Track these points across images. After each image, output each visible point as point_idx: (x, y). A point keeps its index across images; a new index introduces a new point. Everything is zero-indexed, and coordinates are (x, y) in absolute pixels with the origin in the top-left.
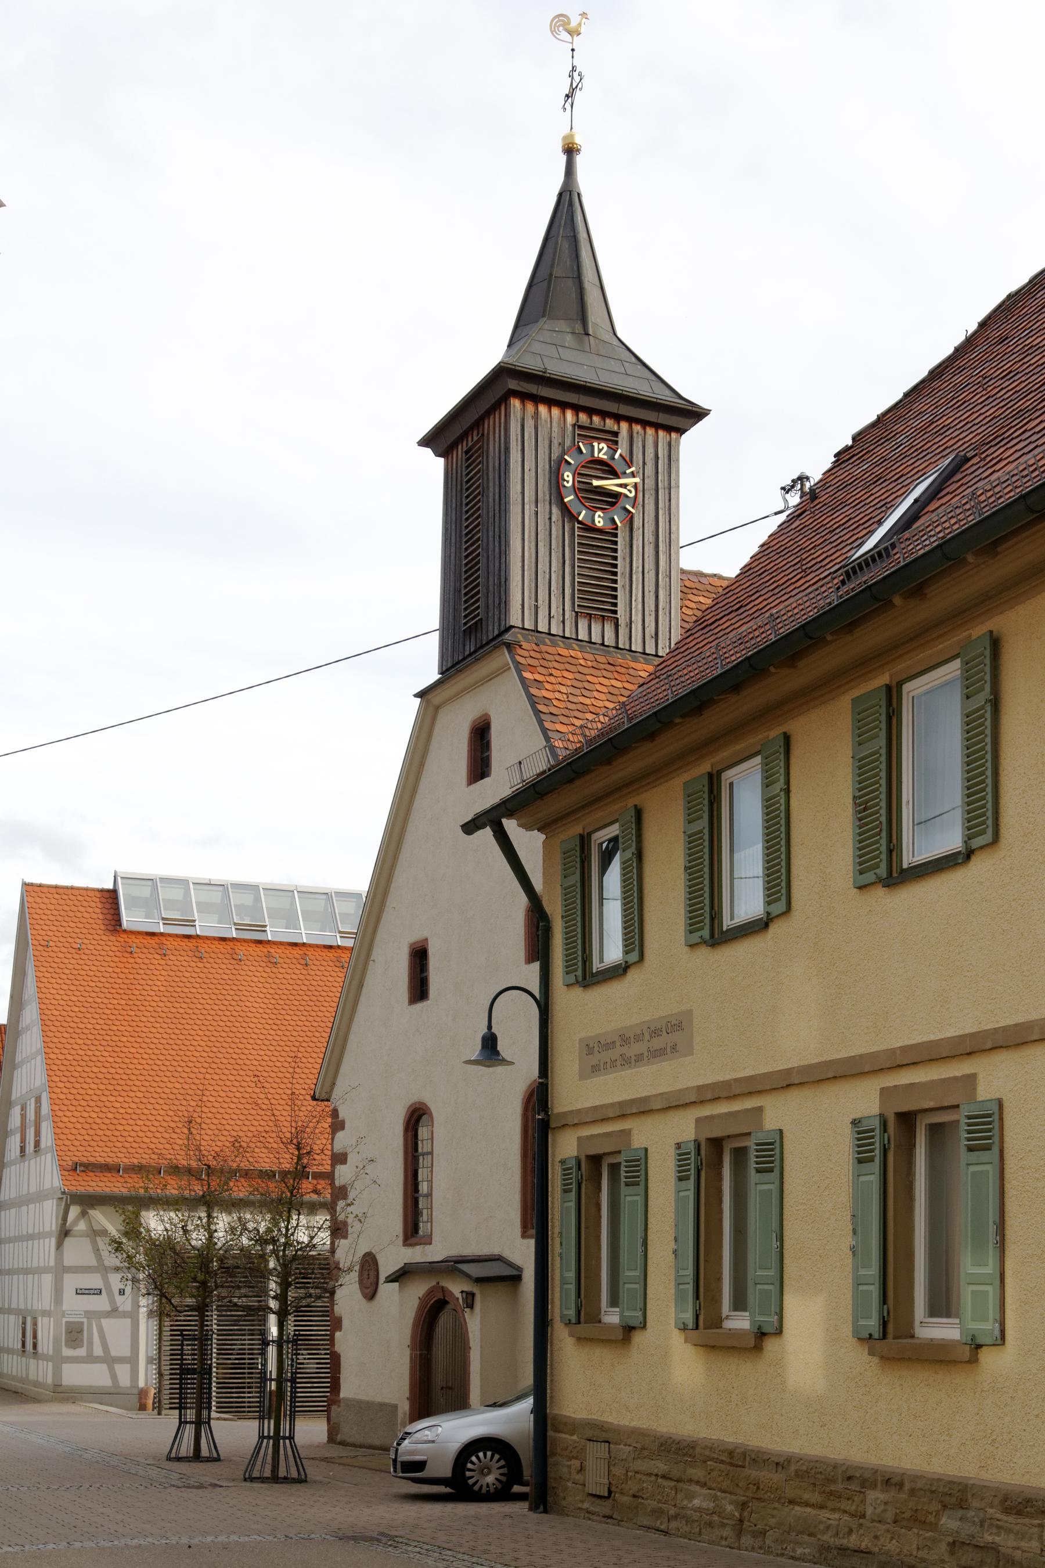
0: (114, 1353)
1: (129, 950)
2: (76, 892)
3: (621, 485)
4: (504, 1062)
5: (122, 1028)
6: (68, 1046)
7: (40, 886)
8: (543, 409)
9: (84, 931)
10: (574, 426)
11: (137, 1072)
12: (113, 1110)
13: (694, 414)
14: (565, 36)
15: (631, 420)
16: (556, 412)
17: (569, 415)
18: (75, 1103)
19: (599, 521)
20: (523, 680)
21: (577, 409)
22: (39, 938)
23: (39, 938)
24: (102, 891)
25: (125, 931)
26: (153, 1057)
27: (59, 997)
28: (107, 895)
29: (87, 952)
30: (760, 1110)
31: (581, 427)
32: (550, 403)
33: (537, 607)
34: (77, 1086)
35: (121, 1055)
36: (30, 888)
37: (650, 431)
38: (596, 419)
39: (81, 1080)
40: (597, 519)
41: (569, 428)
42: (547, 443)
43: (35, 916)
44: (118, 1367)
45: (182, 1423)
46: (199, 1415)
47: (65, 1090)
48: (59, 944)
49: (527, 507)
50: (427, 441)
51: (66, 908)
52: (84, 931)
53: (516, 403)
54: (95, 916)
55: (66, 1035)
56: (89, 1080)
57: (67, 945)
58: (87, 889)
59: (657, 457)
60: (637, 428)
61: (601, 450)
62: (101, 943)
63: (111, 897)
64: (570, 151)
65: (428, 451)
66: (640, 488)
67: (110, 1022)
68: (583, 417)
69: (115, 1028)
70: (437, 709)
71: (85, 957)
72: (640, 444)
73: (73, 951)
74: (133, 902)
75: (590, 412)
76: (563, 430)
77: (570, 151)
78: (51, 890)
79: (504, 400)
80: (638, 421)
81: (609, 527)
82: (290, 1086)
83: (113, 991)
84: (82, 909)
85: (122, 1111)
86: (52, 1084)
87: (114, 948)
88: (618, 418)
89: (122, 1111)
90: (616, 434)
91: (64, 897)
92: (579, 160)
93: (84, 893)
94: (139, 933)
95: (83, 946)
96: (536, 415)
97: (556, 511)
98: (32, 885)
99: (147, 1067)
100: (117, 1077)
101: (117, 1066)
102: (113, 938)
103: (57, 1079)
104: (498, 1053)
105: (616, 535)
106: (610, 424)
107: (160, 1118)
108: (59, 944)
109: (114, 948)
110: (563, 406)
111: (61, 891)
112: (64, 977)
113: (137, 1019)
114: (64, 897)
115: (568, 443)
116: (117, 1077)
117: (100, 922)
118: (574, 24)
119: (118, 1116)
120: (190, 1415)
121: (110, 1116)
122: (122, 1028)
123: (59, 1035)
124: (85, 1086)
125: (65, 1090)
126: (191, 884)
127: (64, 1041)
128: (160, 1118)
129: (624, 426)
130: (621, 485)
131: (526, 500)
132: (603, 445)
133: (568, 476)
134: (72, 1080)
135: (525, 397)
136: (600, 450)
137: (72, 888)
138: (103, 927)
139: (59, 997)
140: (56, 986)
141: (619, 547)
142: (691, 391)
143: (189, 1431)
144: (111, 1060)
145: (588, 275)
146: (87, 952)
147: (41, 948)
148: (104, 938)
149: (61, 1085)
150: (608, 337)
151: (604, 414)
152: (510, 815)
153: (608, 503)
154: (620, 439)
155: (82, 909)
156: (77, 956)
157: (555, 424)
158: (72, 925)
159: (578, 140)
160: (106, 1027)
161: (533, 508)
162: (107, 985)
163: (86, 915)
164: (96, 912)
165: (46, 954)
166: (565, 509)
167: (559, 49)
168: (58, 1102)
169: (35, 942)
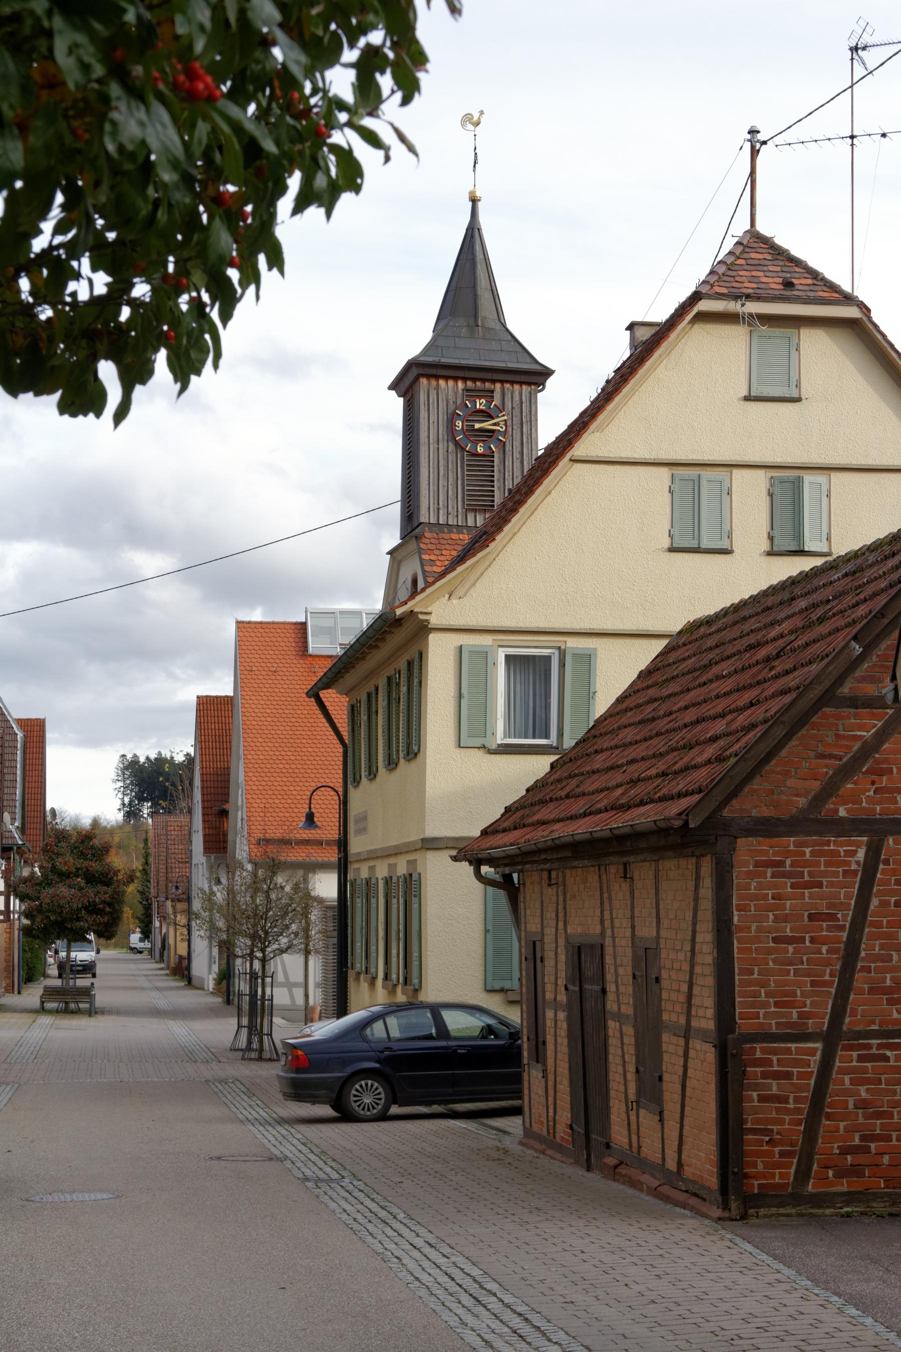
0: (292, 980)
1: (313, 670)
2: (275, 626)
3: (495, 424)
4: (317, 827)
5: (304, 733)
6: (261, 749)
7: (249, 623)
8: (442, 382)
9: (280, 657)
10: (463, 390)
11: (312, 767)
12: (292, 797)
13: (552, 372)
14: (470, 127)
15: (502, 382)
16: (451, 383)
17: (460, 385)
18: (264, 792)
19: (480, 450)
20: (421, 560)
21: (465, 379)
22: (246, 664)
23: (246, 664)
24: (296, 624)
25: (310, 655)
26: (326, 754)
27: (257, 710)
28: (299, 627)
29: (282, 673)
30: (415, 861)
31: (468, 390)
32: (446, 378)
33: (438, 509)
34: (266, 779)
35: (301, 754)
36: (241, 625)
37: (517, 387)
38: (478, 384)
39: (269, 774)
40: (479, 449)
41: (460, 391)
42: (445, 403)
43: (244, 647)
44: (294, 990)
45: (240, 1026)
46: (250, 1021)
47: (257, 783)
48: (261, 669)
49: (431, 446)
50: (391, 388)
51: (268, 639)
52: (280, 657)
53: (424, 381)
54: (289, 644)
55: (260, 740)
56: (275, 775)
57: (266, 669)
58: (284, 623)
59: (521, 403)
60: (507, 386)
61: (480, 404)
62: (292, 665)
63: (302, 627)
64: (474, 201)
65: (393, 393)
66: (509, 423)
67: (295, 728)
68: (470, 384)
69: (298, 733)
70: (400, 562)
71: (279, 678)
72: (510, 396)
73: (270, 673)
74: (319, 631)
75: (474, 380)
76: (456, 393)
77: (474, 201)
78: (257, 626)
79: (417, 379)
80: (507, 382)
81: (488, 452)
82: (262, 823)
83: (299, 703)
84: (279, 639)
85: (299, 797)
86: (248, 779)
87: (302, 670)
88: (494, 381)
89: (299, 797)
90: (492, 392)
91: (267, 630)
92: (480, 205)
93: (282, 626)
94: (322, 656)
95: (279, 669)
96: (437, 387)
97: (452, 447)
98: (243, 622)
99: (320, 762)
100: (297, 771)
101: (297, 762)
102: (302, 662)
103: (251, 774)
104: (314, 822)
105: (493, 457)
106: (488, 385)
107: (327, 802)
108: (261, 669)
109: (302, 670)
110: (456, 379)
111: (264, 626)
112: (262, 694)
113: (315, 725)
114: (267, 630)
115: (459, 401)
116: (297, 771)
117: (292, 649)
118: (476, 118)
119: (295, 801)
120: (245, 1021)
121: (289, 801)
122: (304, 733)
123: (255, 740)
124: (272, 779)
125: (257, 783)
126: (364, 615)
127: (258, 744)
128: (327, 802)
129: (498, 386)
130: (495, 424)
131: (431, 441)
132: (483, 401)
133: (459, 424)
134: (263, 774)
135: (429, 376)
136: (480, 404)
137: (273, 623)
138: (294, 653)
139: (257, 710)
140: (256, 702)
141: (495, 464)
142: (544, 357)
143: (244, 1032)
144: (293, 758)
145: (482, 282)
146: (282, 673)
147: (246, 672)
148: (295, 661)
149: (254, 779)
150: (493, 324)
151: (484, 381)
152: (327, 686)
153: (487, 436)
154: (495, 394)
155: (279, 639)
156: (273, 677)
157: (450, 391)
158: (271, 652)
159: (478, 194)
160: (291, 732)
161: (436, 445)
162: (294, 699)
163: (283, 644)
164: (290, 641)
165: (249, 677)
166: (457, 444)
167: (466, 136)
168: (251, 792)
169: (243, 668)
